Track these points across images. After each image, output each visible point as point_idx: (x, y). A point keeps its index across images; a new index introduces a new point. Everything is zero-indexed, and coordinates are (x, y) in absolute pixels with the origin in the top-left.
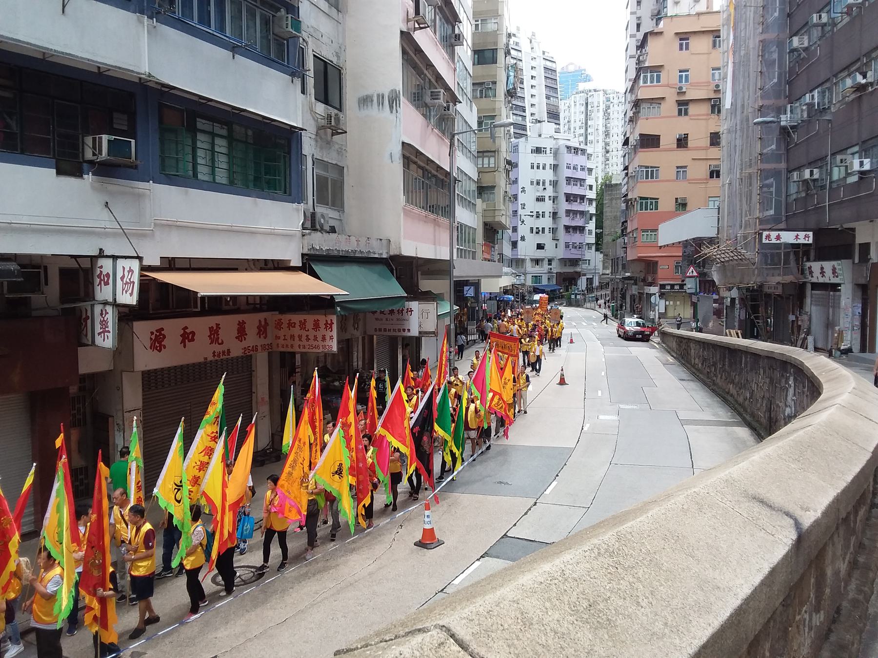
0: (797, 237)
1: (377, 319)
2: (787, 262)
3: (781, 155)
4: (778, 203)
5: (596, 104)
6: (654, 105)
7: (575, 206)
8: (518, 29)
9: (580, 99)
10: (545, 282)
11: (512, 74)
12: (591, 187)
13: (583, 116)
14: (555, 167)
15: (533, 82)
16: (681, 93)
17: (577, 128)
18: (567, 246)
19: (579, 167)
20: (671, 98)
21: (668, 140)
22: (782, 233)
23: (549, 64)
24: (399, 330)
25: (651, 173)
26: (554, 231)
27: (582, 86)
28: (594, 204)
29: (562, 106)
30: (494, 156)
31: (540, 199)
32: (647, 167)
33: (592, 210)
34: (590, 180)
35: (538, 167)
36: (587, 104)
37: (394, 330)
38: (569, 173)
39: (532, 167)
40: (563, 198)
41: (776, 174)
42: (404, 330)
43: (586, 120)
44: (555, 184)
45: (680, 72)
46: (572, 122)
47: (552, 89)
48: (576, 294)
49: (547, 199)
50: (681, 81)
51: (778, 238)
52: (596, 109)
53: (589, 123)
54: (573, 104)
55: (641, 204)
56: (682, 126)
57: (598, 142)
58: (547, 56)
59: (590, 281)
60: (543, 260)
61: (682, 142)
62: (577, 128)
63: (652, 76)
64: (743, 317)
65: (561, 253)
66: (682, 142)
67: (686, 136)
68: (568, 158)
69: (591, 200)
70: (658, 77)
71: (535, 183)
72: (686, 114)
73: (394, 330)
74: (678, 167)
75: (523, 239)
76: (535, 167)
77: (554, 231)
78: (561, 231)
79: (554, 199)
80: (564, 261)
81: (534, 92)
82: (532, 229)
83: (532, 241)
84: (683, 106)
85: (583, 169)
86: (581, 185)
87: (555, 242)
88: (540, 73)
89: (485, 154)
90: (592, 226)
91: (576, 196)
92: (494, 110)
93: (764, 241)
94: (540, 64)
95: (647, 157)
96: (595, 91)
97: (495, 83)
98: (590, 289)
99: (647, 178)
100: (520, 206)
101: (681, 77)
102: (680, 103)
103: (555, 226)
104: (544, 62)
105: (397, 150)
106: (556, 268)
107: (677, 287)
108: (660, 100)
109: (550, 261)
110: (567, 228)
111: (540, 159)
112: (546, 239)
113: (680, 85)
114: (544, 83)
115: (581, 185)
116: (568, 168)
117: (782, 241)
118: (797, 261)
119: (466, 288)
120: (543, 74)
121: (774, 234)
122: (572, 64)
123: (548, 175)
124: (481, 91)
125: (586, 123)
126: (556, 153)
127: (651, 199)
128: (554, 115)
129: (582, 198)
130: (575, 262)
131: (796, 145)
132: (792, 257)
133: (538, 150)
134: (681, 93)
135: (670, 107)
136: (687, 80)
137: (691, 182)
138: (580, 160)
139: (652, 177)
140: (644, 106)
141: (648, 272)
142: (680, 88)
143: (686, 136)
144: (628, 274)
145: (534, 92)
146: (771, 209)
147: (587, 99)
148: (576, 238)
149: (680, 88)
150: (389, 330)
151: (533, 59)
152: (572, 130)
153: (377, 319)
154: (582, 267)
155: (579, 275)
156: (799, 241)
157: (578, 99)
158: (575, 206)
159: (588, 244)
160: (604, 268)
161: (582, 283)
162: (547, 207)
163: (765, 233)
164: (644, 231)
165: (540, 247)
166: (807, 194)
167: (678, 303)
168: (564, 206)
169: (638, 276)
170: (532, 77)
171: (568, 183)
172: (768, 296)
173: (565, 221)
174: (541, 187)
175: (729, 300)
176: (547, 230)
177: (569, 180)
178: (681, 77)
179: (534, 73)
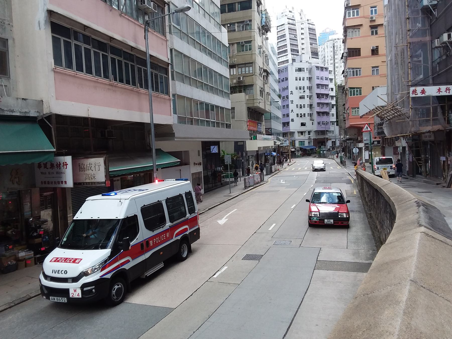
0: (439, 90)
1: (42, 173)
2: (435, 114)
3: (427, 29)
4: (426, 69)
5: (339, 46)
6: (356, 30)
7: (323, 101)
8: (293, 8)
9: (330, 44)
10: (306, 144)
11: (264, 16)
12: (332, 89)
13: (332, 54)
14: (310, 79)
15: (303, 36)
16: (372, 21)
17: (329, 60)
18: (319, 123)
19: (324, 78)
20: (366, 24)
21: (366, 51)
22: (426, 88)
23: (311, 26)
24: (59, 183)
25: (356, 72)
26: (311, 115)
27: (331, 37)
28: (335, 99)
29: (320, 49)
30: (252, 66)
31: (302, 97)
32: (353, 69)
33: (334, 102)
34: (332, 85)
35: (300, 79)
36: (334, 47)
37: (55, 183)
38: (319, 82)
39: (296, 80)
40: (315, 96)
41: (423, 45)
42: (62, 182)
43: (334, 56)
44: (310, 88)
45: (371, 8)
46: (326, 57)
47: (313, 39)
48: (323, 151)
49: (306, 97)
50: (372, 13)
51: (423, 92)
52: (339, 49)
53: (336, 57)
54: (326, 47)
55: (351, 92)
56: (374, 41)
57: (341, 67)
58: (309, 22)
59: (334, 143)
60: (305, 132)
61: (375, 52)
62: (329, 60)
63: (353, 12)
64: (411, 160)
65: (315, 127)
66: (375, 52)
67: (377, 47)
68: (318, 73)
69: (332, 97)
70: (357, 12)
71: (298, 88)
72: (376, 33)
73: (55, 183)
74: (373, 67)
75: (293, 120)
76: (298, 79)
77: (311, 115)
78: (315, 115)
79: (310, 97)
80: (317, 132)
81: (303, 41)
82: (298, 115)
83: (298, 121)
84: (374, 28)
85: (326, 79)
86: (326, 88)
87: (312, 121)
88: (306, 31)
89: (247, 65)
90: (334, 111)
91: (323, 95)
92: (251, 37)
93: (411, 95)
94: (306, 26)
95: (354, 62)
96: (338, 39)
97: (250, 21)
98: (333, 148)
99: (354, 75)
100: (290, 102)
101: (372, 11)
102: (372, 27)
103: (311, 113)
104: (308, 25)
105: (41, 16)
106: (313, 136)
107: (376, 143)
108: (358, 26)
109: (309, 133)
110: (318, 113)
111: (301, 75)
112: (306, 120)
113: (371, 16)
114: (309, 37)
115: (326, 88)
116: (318, 79)
117: (427, 94)
118: (444, 113)
119: (212, 147)
120: (308, 32)
121: (419, 89)
122: (328, 28)
123: (306, 83)
124: (243, 27)
125: (334, 57)
126: (310, 71)
127: (357, 88)
128: (315, 54)
129: (327, 95)
130: (323, 132)
131: (437, 18)
132: (439, 110)
133: (300, 70)
134: (372, 21)
135: (366, 29)
136: (376, 13)
137: (382, 76)
138: (324, 74)
139: (357, 75)
140: (349, 31)
141: (359, 135)
142: (372, 18)
143: (377, 47)
144: (348, 137)
145: (303, 41)
146: (421, 74)
147: (334, 44)
148: (324, 119)
149: (372, 18)
150: (48, 183)
151: (302, 24)
152: (326, 61)
153: (42, 173)
154: (329, 135)
155: (328, 139)
156: (441, 94)
157: (329, 44)
158: (323, 101)
159: (332, 122)
160: (340, 134)
161: (329, 144)
162: (306, 101)
163: (412, 89)
164: (353, 108)
165: (303, 124)
166: (447, 56)
167: (377, 153)
168: (316, 100)
169: (354, 137)
170: (302, 34)
171: (318, 88)
172: (425, 143)
173: (317, 109)
174: (302, 91)
175: (401, 148)
176: (306, 115)
177: (318, 86)
178: (372, 11)
179: (303, 31)
